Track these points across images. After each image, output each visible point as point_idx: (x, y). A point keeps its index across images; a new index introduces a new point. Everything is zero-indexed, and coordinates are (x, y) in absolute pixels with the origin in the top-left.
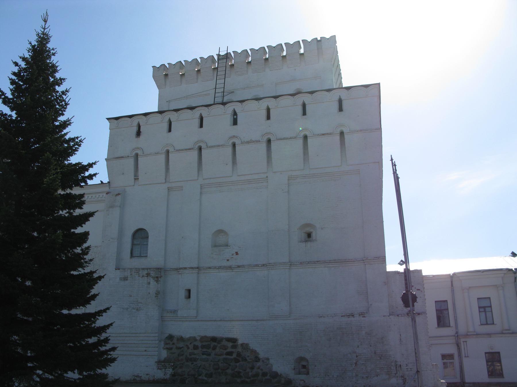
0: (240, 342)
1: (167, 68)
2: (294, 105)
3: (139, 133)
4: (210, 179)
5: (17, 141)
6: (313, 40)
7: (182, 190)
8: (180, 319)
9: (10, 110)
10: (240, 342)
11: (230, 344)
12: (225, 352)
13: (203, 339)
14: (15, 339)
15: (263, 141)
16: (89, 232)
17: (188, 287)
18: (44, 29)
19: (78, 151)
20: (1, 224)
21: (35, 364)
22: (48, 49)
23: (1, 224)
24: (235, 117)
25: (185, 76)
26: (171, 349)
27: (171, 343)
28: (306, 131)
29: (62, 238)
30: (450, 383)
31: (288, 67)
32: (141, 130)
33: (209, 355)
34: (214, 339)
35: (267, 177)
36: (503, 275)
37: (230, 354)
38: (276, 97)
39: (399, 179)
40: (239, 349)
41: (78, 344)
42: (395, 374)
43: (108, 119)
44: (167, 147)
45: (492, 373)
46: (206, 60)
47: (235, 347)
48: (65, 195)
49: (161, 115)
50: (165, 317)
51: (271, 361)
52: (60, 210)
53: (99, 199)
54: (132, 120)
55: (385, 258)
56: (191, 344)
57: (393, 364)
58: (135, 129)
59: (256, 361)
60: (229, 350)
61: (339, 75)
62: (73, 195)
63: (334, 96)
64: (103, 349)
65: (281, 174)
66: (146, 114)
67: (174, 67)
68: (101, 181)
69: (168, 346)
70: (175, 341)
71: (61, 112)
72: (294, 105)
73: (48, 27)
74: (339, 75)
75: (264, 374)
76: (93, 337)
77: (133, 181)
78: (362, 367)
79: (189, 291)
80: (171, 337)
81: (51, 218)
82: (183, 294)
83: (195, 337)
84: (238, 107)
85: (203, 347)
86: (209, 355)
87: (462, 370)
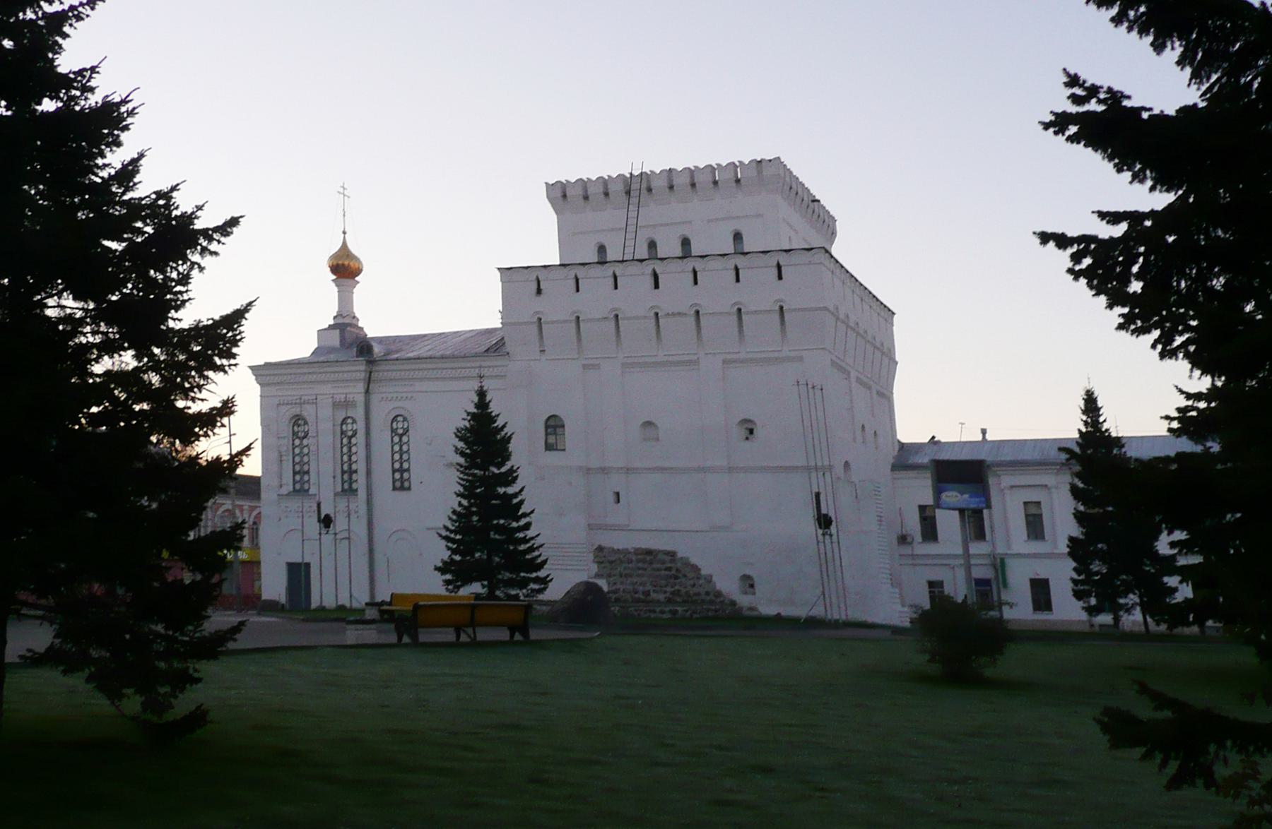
3: (539, 291)
6: (577, 181)
11: (668, 558)
13: (638, 552)
17: (616, 490)
20: (1092, 450)
23: (1092, 450)
26: (602, 563)
32: (541, 287)
33: (645, 569)
34: (649, 552)
35: (698, 359)
37: (669, 569)
40: (679, 565)
41: (1111, 283)
43: (499, 269)
47: (673, 561)
51: (714, 579)
58: (535, 286)
60: (669, 565)
61: (833, 234)
62: (505, 462)
63: (772, 260)
66: (545, 267)
74: (833, 234)
75: (707, 593)
79: (618, 494)
80: (600, 549)
82: (612, 498)
83: (627, 549)
84: (659, 267)
85: (638, 561)
86: (625, 568)
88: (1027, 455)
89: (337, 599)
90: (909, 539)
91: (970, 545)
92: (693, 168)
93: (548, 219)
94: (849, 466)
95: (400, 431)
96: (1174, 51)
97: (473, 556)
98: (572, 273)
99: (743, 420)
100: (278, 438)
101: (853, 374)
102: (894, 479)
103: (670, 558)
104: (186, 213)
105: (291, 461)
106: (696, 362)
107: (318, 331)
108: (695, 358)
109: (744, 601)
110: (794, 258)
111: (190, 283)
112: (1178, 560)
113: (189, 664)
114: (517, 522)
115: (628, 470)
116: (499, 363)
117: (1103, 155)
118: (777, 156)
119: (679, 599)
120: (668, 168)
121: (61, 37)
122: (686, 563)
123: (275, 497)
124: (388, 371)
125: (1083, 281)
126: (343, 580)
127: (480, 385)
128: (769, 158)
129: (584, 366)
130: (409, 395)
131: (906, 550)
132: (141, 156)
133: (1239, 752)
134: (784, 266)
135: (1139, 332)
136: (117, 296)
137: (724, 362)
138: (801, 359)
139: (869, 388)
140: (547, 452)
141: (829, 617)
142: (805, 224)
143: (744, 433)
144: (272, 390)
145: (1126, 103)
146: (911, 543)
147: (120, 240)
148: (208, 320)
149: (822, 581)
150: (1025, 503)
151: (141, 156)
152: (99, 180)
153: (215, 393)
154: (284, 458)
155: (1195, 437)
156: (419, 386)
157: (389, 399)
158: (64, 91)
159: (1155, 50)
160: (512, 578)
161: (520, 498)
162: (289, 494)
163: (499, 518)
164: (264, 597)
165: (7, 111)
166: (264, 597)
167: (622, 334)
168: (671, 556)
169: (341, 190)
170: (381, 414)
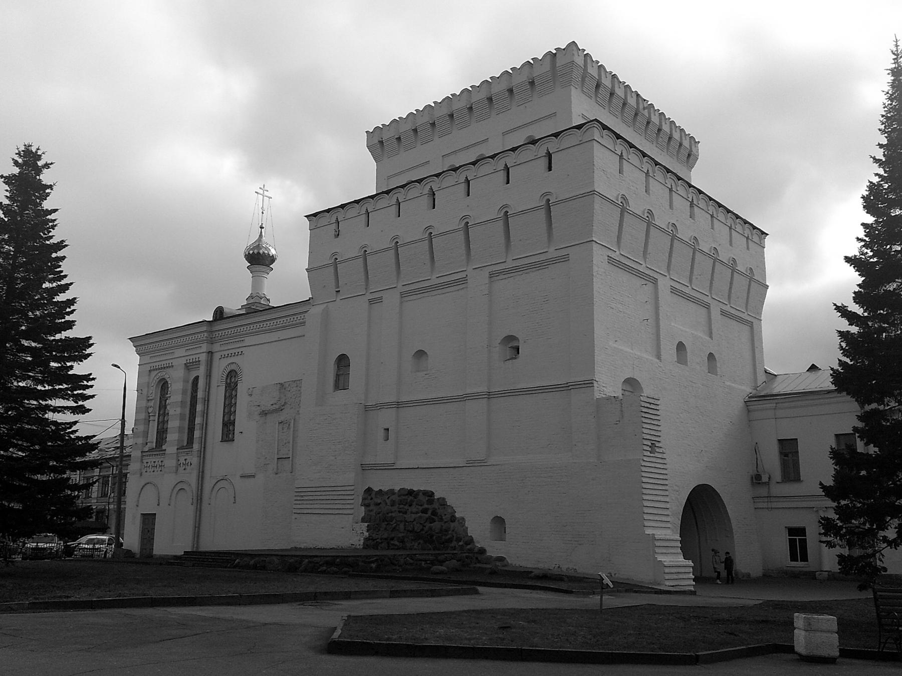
0: (437, 496)
1: (489, 82)
2: (440, 189)
4: (659, 546)
5: (43, 432)
7: (382, 302)
8: (636, 272)
9: (887, 88)
10: (437, 496)
12: (421, 508)
14: (448, 568)
15: (188, 357)
16: (273, 259)
17: (158, 506)
18: (54, 185)
19: (858, 285)
21: (59, 443)
22: (47, 411)
24: (194, 394)
25: (494, 101)
27: (369, 498)
28: (706, 202)
29: (73, 495)
30: (356, 618)
31: (362, 467)
34: (411, 492)
35: (467, 275)
36: (775, 405)
37: (425, 511)
38: (556, 135)
39: (829, 482)
40: (436, 505)
41: (49, 496)
42: (254, 647)
44: (545, 196)
45: (723, 563)
46: (422, 113)
48: (79, 536)
49: (535, 146)
50: (699, 534)
52: (138, 556)
53: (187, 342)
54: (536, 148)
55: (730, 582)
56: (388, 498)
57: (870, 551)
59: (452, 521)
60: (426, 506)
64: (59, 298)
65: (481, 270)
66: (342, 206)
67: (478, 91)
68: (91, 410)
69: (367, 502)
70: (373, 495)
71: (14, 304)
72: (440, 189)
73: (142, 489)
76: (831, 486)
77: (335, 294)
78: (709, 636)
79: (343, 361)
81: (15, 426)
82: (381, 434)
87: (210, 373)
88: (122, 523)
89: (197, 527)
90: (765, 479)
91: (763, 481)
92: (554, 52)
93: (371, 165)
94: (643, 390)
95: (232, 379)
96: (47, 205)
97: (56, 354)
98: (392, 199)
99: (494, 517)
100: (148, 400)
101: (664, 284)
102: (402, 297)
103: (604, 271)
104: (859, 275)
105: (157, 421)
106: (464, 280)
107: (574, 42)
108: (463, 275)
109: (494, 549)
110: (567, 141)
111: (61, 246)
112: (868, 590)
113: (398, 498)
114: (88, 382)
115: (398, 405)
116: (340, 603)
117: (891, 81)
118: (811, 364)
119: (280, 662)
120: (309, 231)
121: (603, 398)
122: (442, 502)
123: (139, 454)
124: (338, 604)
125: (882, 150)
126: (651, 517)
127: (53, 184)
128: (645, 99)
129: (371, 302)
130: (240, 350)
131: (763, 491)
132: (71, 284)
133: (43, 475)
134: (832, 632)
135: (845, 352)
136: (880, 536)
137: (491, 275)
138: (565, 259)
139: (707, 307)
140: (802, 479)
141: (489, 527)
142: (466, 663)
143: (509, 353)
144: (147, 359)
145: (43, 183)
146: (767, 484)
147: (18, 427)
148: (879, 566)
149: (840, 402)
150: (837, 435)
151: (71, 284)
152: (897, 280)
153: (119, 367)
154: (151, 418)
155: (856, 268)
156: (249, 341)
157: (236, 354)
158: (895, 477)
159: (73, 367)
160: (60, 281)
161: (60, 254)
162: (151, 450)
163: (24, 486)
164: (860, 280)
165: (851, 361)
166: (860, 280)
167: (472, 253)
168: (429, 496)
169: (261, 191)
170: (220, 368)
